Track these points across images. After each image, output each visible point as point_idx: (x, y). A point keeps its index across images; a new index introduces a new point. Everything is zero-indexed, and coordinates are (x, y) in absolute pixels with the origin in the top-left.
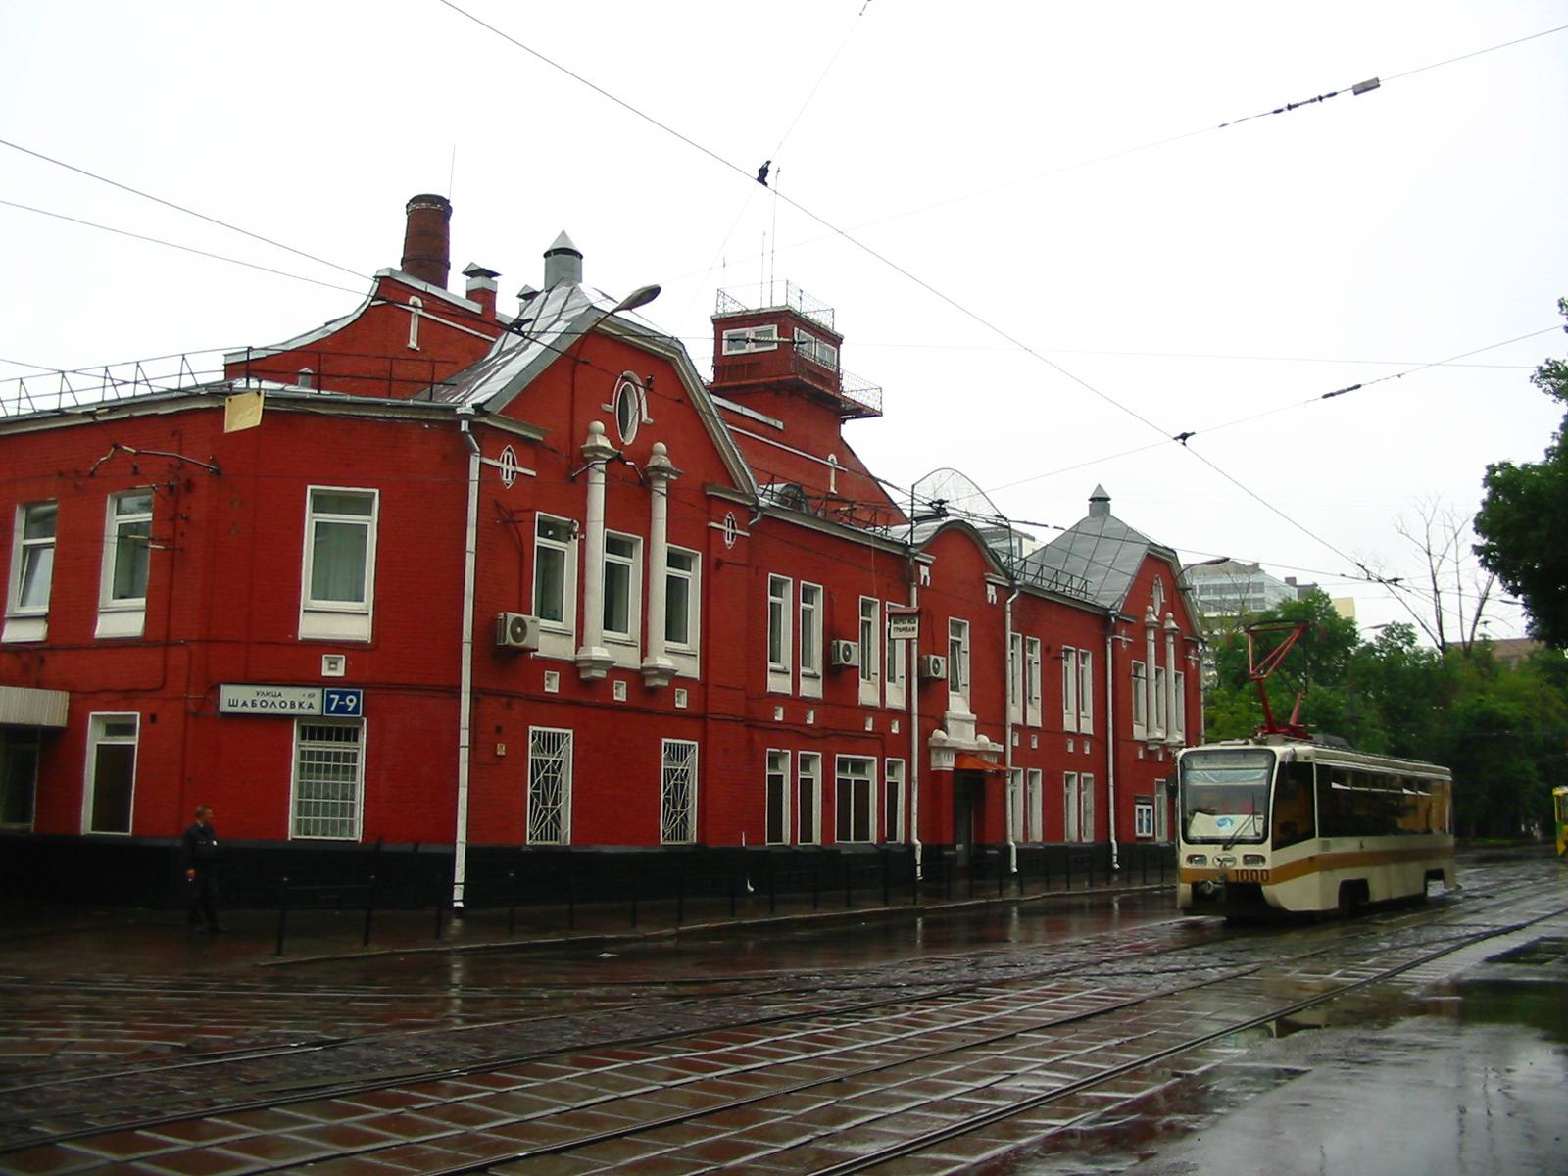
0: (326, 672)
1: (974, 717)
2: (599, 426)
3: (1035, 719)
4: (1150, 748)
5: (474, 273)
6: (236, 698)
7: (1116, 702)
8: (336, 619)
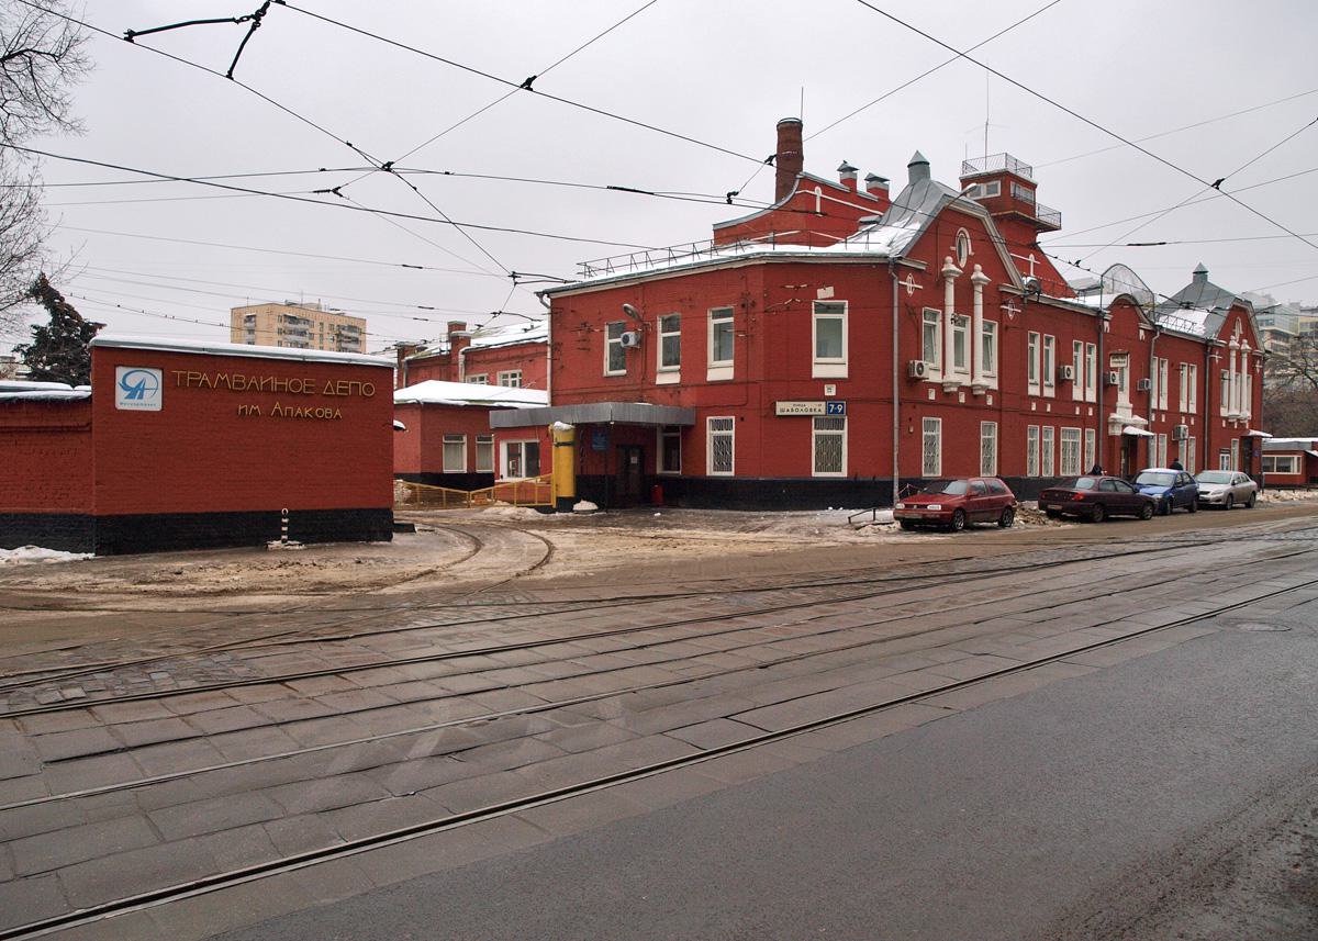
0: (826, 394)
1: (1131, 405)
2: (949, 259)
3: (1164, 406)
4: (975, 393)
5: (871, 179)
6: (784, 408)
7: (1210, 394)
8: (831, 367)
